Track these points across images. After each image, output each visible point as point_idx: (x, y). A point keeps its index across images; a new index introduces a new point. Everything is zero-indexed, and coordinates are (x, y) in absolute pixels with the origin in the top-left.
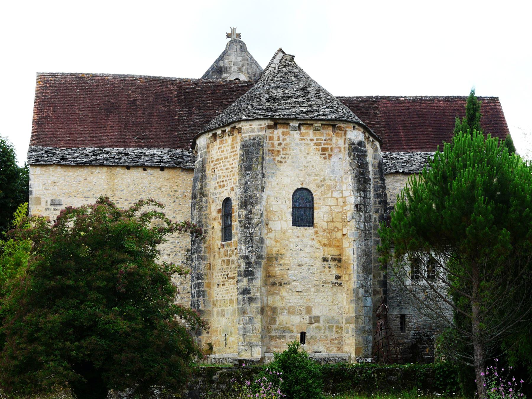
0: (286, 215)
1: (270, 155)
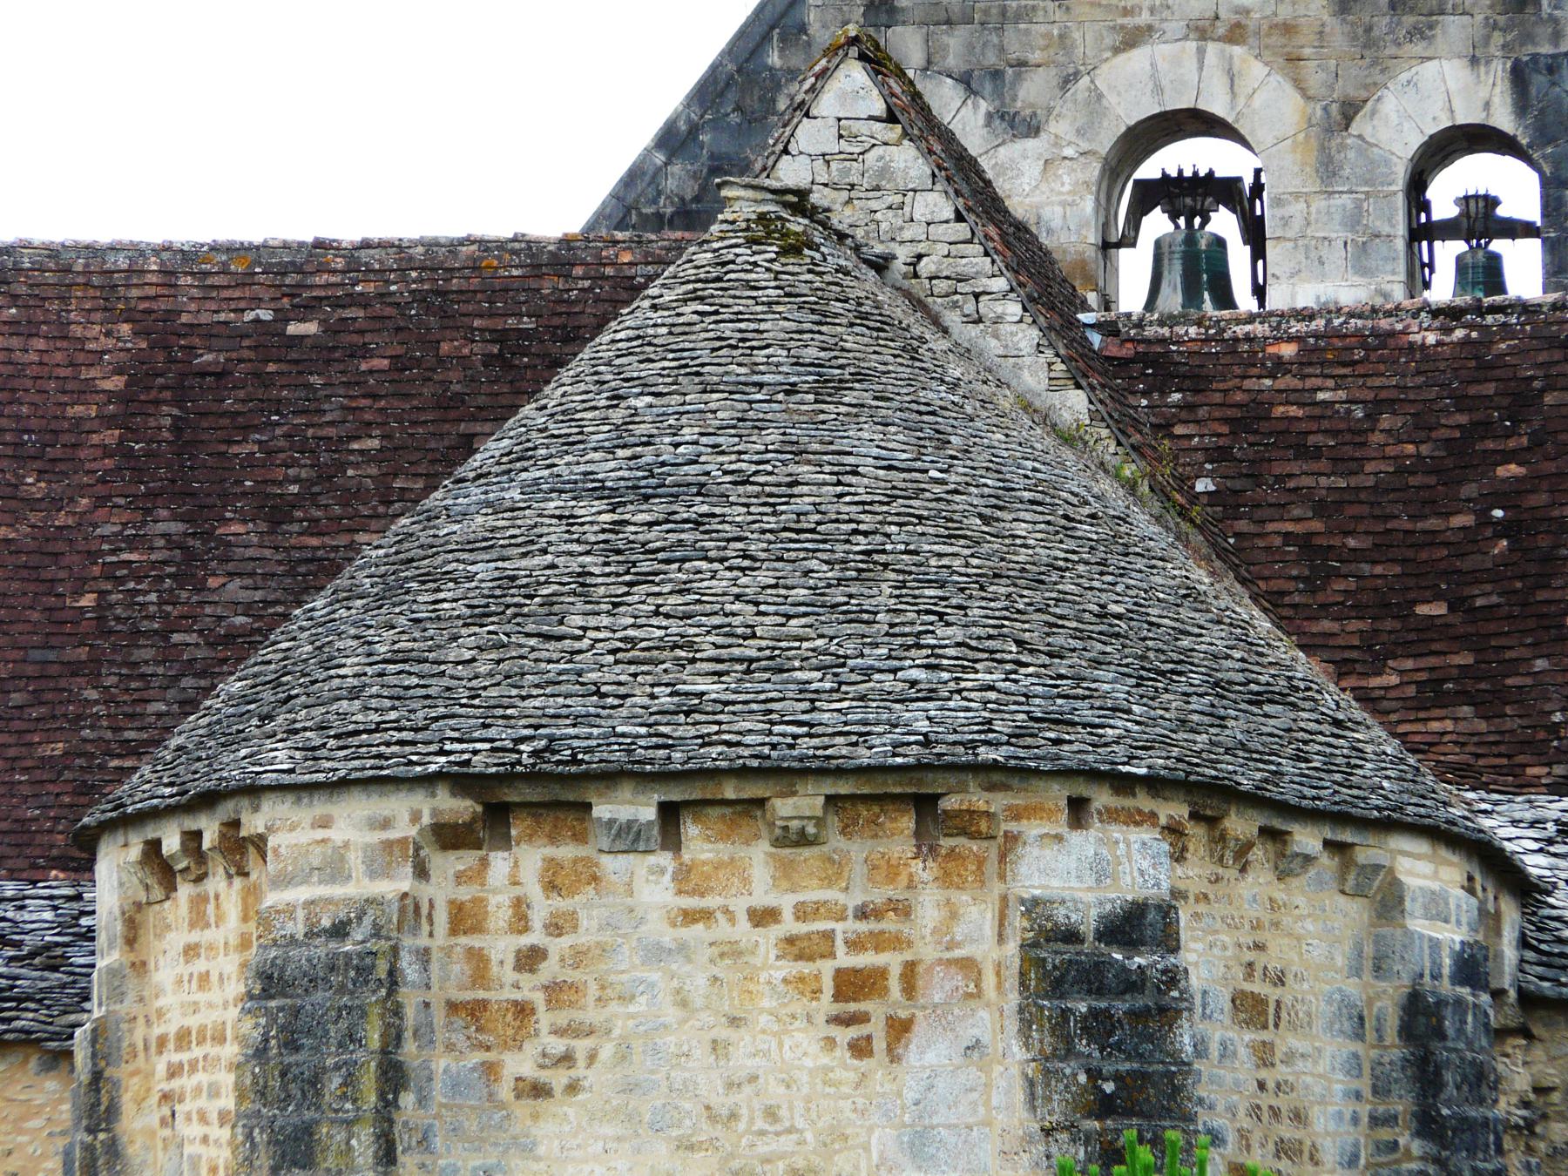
1: (459, 1039)
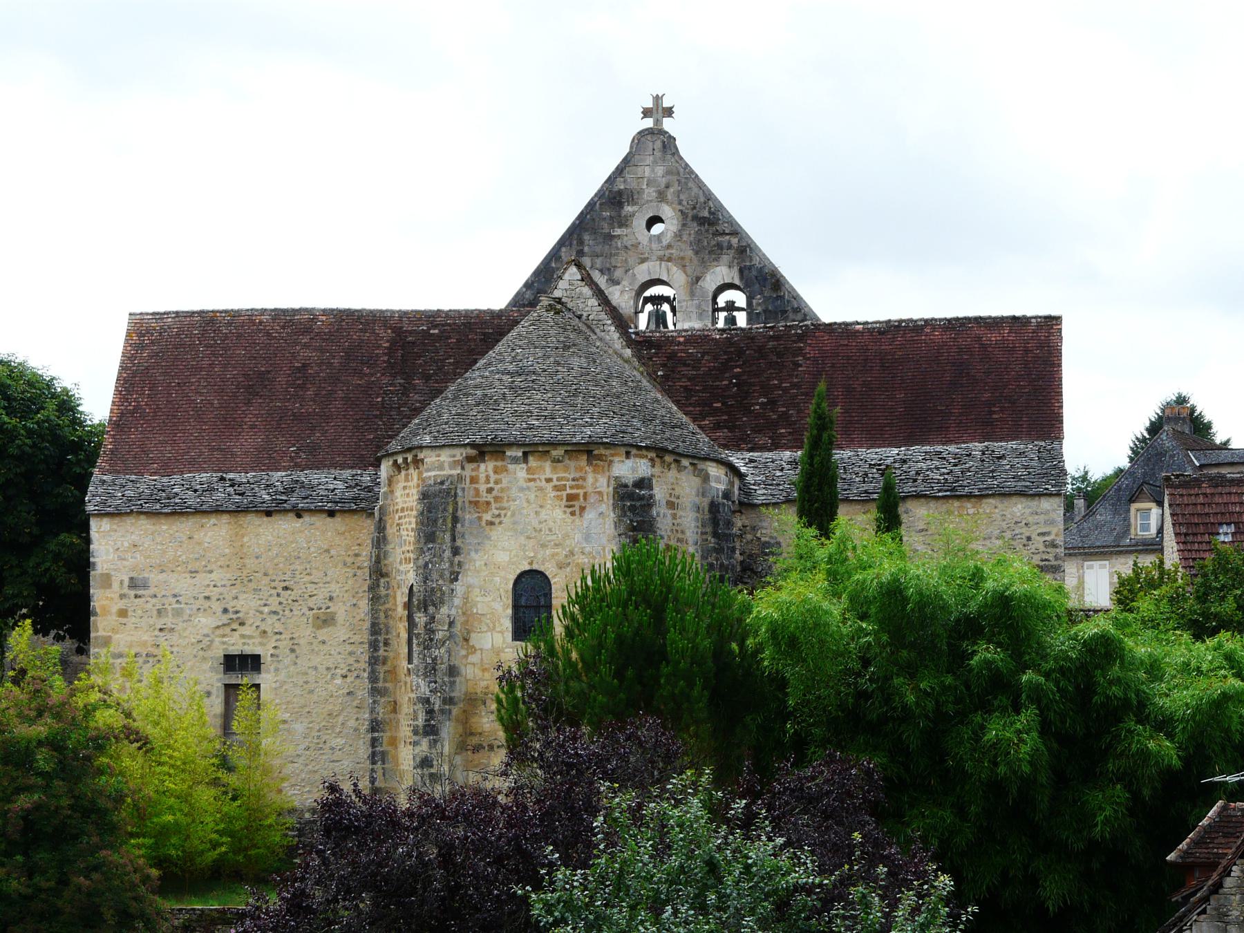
0: (502, 621)
